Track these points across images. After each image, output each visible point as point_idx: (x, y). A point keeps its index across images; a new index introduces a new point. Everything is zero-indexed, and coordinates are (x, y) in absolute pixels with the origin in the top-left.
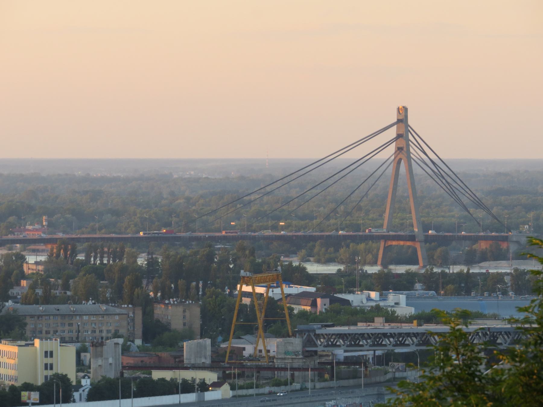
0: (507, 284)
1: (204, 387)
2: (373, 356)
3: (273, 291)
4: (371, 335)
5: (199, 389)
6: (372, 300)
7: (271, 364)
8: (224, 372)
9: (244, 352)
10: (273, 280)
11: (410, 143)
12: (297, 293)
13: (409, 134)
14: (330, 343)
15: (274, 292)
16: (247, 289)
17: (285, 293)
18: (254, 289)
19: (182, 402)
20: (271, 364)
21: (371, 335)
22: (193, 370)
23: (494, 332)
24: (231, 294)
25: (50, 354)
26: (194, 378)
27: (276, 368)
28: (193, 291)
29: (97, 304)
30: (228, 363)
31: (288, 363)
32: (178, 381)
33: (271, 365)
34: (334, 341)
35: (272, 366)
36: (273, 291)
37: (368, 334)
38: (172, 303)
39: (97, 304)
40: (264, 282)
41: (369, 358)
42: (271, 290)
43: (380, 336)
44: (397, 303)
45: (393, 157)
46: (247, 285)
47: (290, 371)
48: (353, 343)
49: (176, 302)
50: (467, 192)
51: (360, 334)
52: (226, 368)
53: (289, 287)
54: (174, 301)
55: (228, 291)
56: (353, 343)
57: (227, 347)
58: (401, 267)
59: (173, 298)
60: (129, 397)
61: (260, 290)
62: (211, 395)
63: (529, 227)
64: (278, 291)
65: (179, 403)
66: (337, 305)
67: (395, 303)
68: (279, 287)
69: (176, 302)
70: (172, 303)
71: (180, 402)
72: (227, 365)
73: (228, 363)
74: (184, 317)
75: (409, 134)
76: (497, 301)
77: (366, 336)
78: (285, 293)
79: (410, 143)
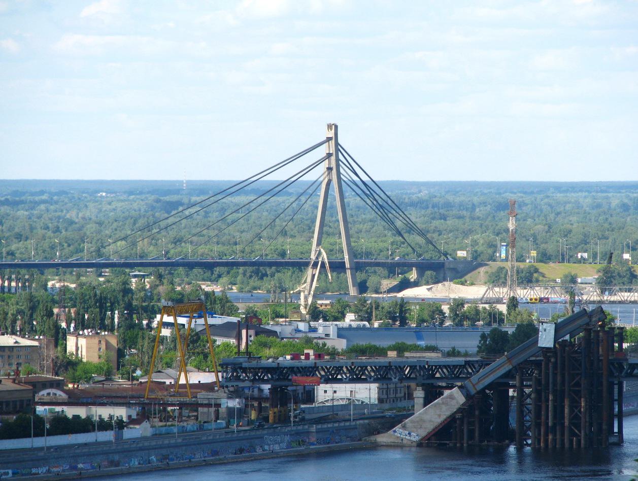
0: (445, 313)
1: (121, 425)
2: (302, 391)
3: (196, 322)
4: (301, 369)
5: (117, 426)
6: (300, 331)
7: (194, 399)
8: (144, 408)
9: (270, 387)
10: (195, 311)
11: (340, 162)
12: (220, 323)
13: (339, 153)
14: (257, 377)
15: (197, 323)
16: (168, 319)
17: (208, 323)
18: (176, 320)
19: (98, 440)
20: (194, 399)
21: (301, 369)
22: (111, 406)
23: (432, 366)
24: (149, 325)
25: (505, 383)
26: (112, 414)
27: (199, 404)
28: (107, 322)
29: (6, 335)
30: (147, 398)
31: (212, 399)
32: (95, 418)
33: (194, 401)
34: (261, 376)
35: (195, 403)
36: (196, 322)
37: (298, 368)
38: (87, 334)
39: (6, 335)
40: (187, 312)
41: (298, 394)
42: (193, 320)
43: (310, 369)
44: (328, 335)
45: (365, 178)
46: (169, 315)
47: (214, 407)
48: (355, 377)
49: (90, 334)
50: (386, 214)
51: (290, 368)
52: (145, 403)
53: (212, 317)
54: (89, 333)
55: (145, 322)
56: (355, 377)
57: (147, 382)
58: (465, 296)
59: (88, 329)
60: (43, 435)
61: (182, 320)
62: (130, 433)
63: (467, 252)
64: (201, 321)
65: (95, 441)
66: (263, 338)
67: (326, 335)
68: (202, 317)
69: (90, 334)
70: (87, 334)
71: (96, 440)
72: (146, 401)
73: (147, 398)
74: (100, 349)
75: (339, 153)
76: (435, 332)
77: (295, 369)
78: (208, 323)
79: (340, 162)
